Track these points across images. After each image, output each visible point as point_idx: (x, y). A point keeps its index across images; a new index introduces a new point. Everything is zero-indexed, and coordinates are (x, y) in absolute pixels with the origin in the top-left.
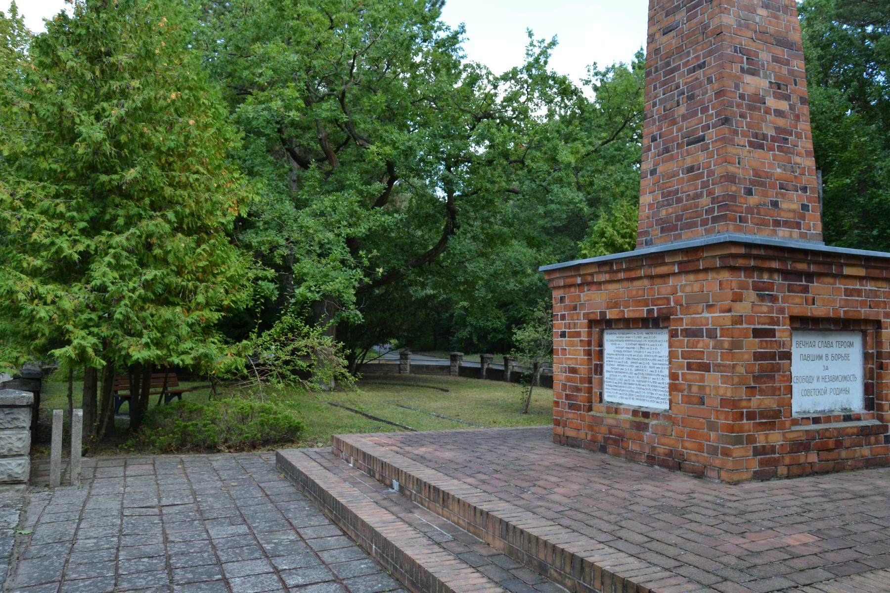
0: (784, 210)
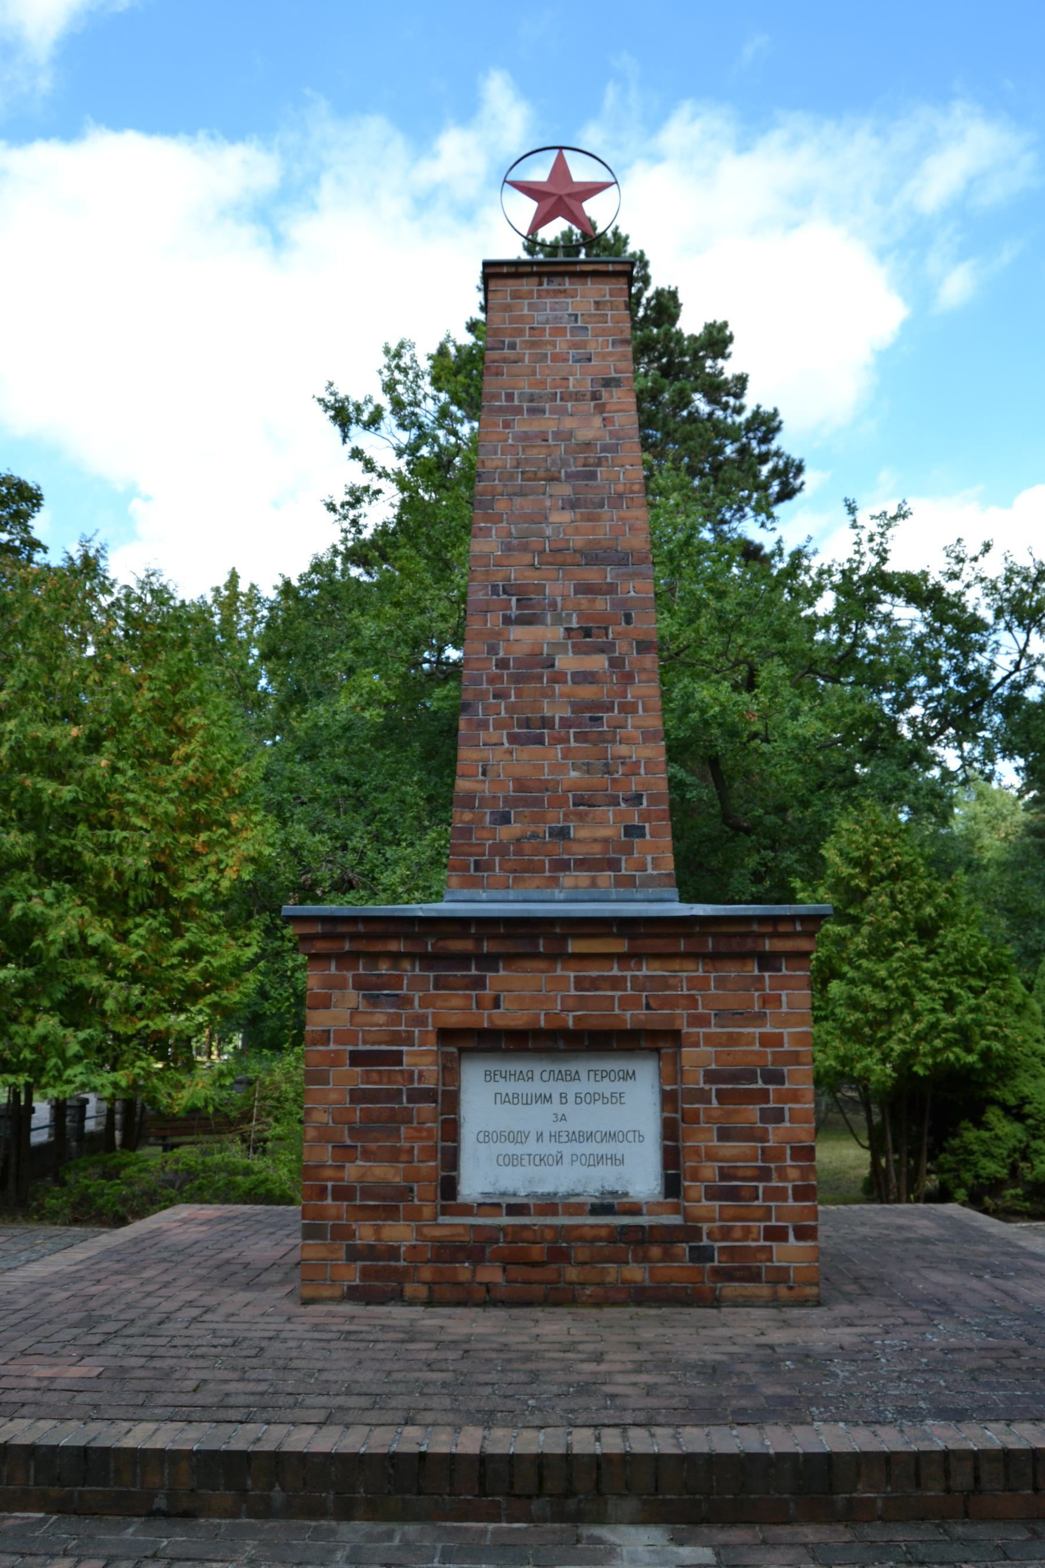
0: (579, 841)
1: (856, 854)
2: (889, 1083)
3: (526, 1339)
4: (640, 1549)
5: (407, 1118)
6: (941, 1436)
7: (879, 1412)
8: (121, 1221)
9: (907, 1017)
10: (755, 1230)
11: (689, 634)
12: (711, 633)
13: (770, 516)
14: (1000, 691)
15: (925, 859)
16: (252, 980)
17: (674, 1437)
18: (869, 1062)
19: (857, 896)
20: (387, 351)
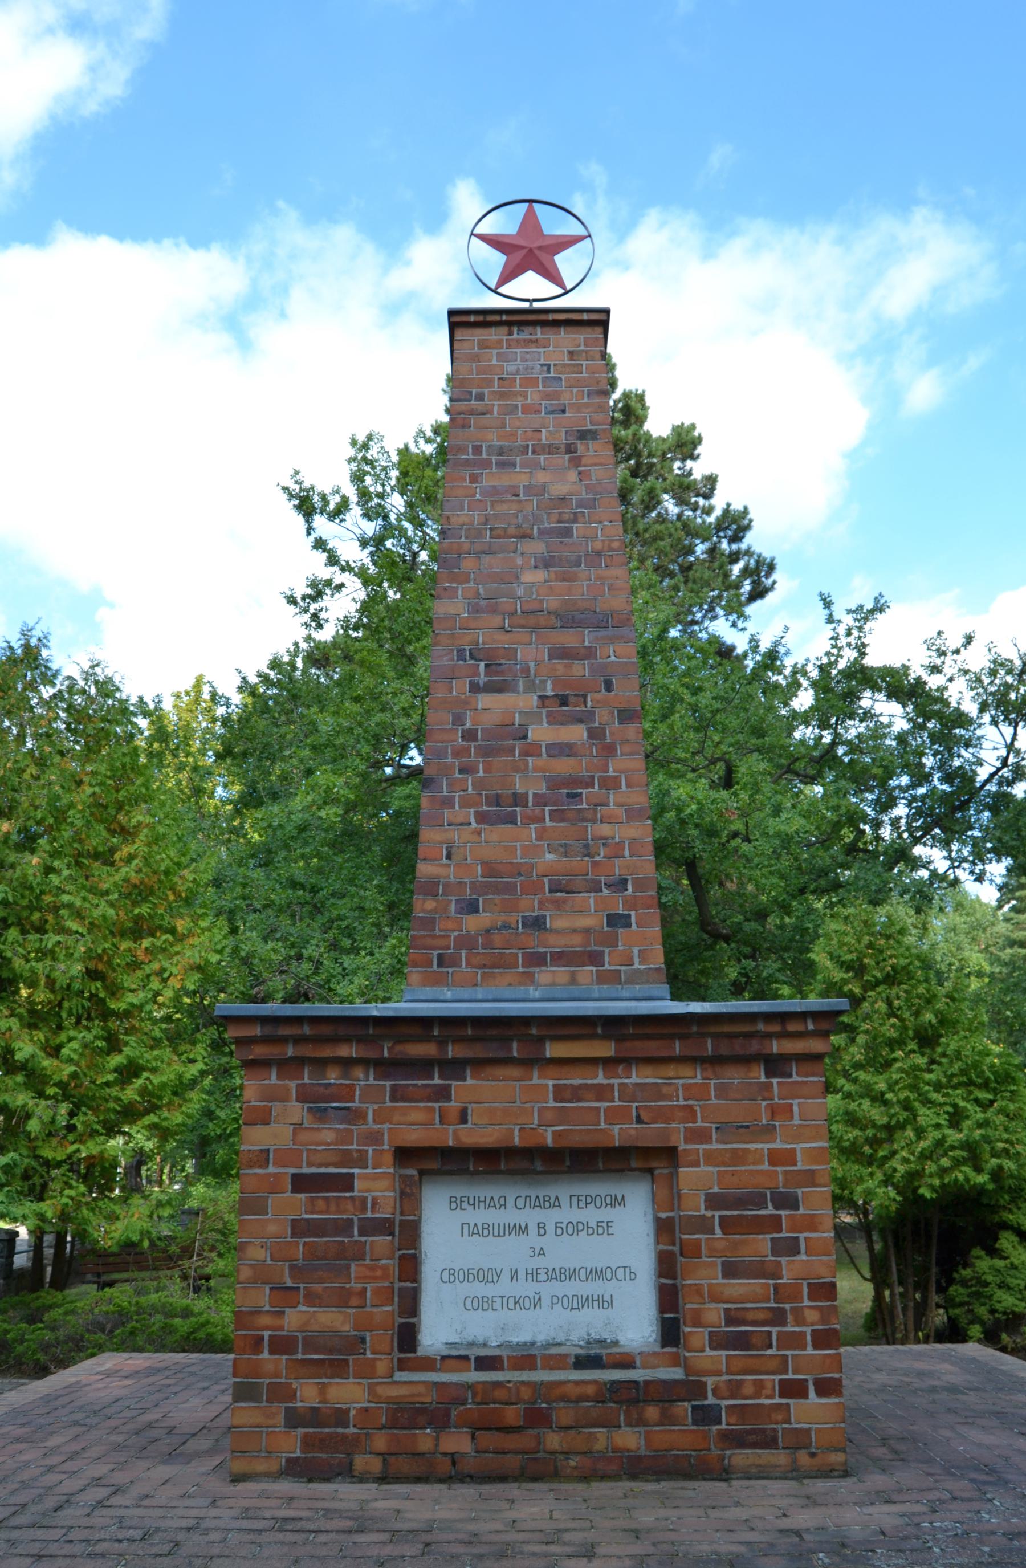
2: (893, 1207)
3: (499, 1526)
8: (42, 1371)
9: (909, 1133)
10: (769, 1385)
13: (741, 615)
14: (987, 787)
16: (196, 1100)
18: (870, 1184)
20: (354, 443)
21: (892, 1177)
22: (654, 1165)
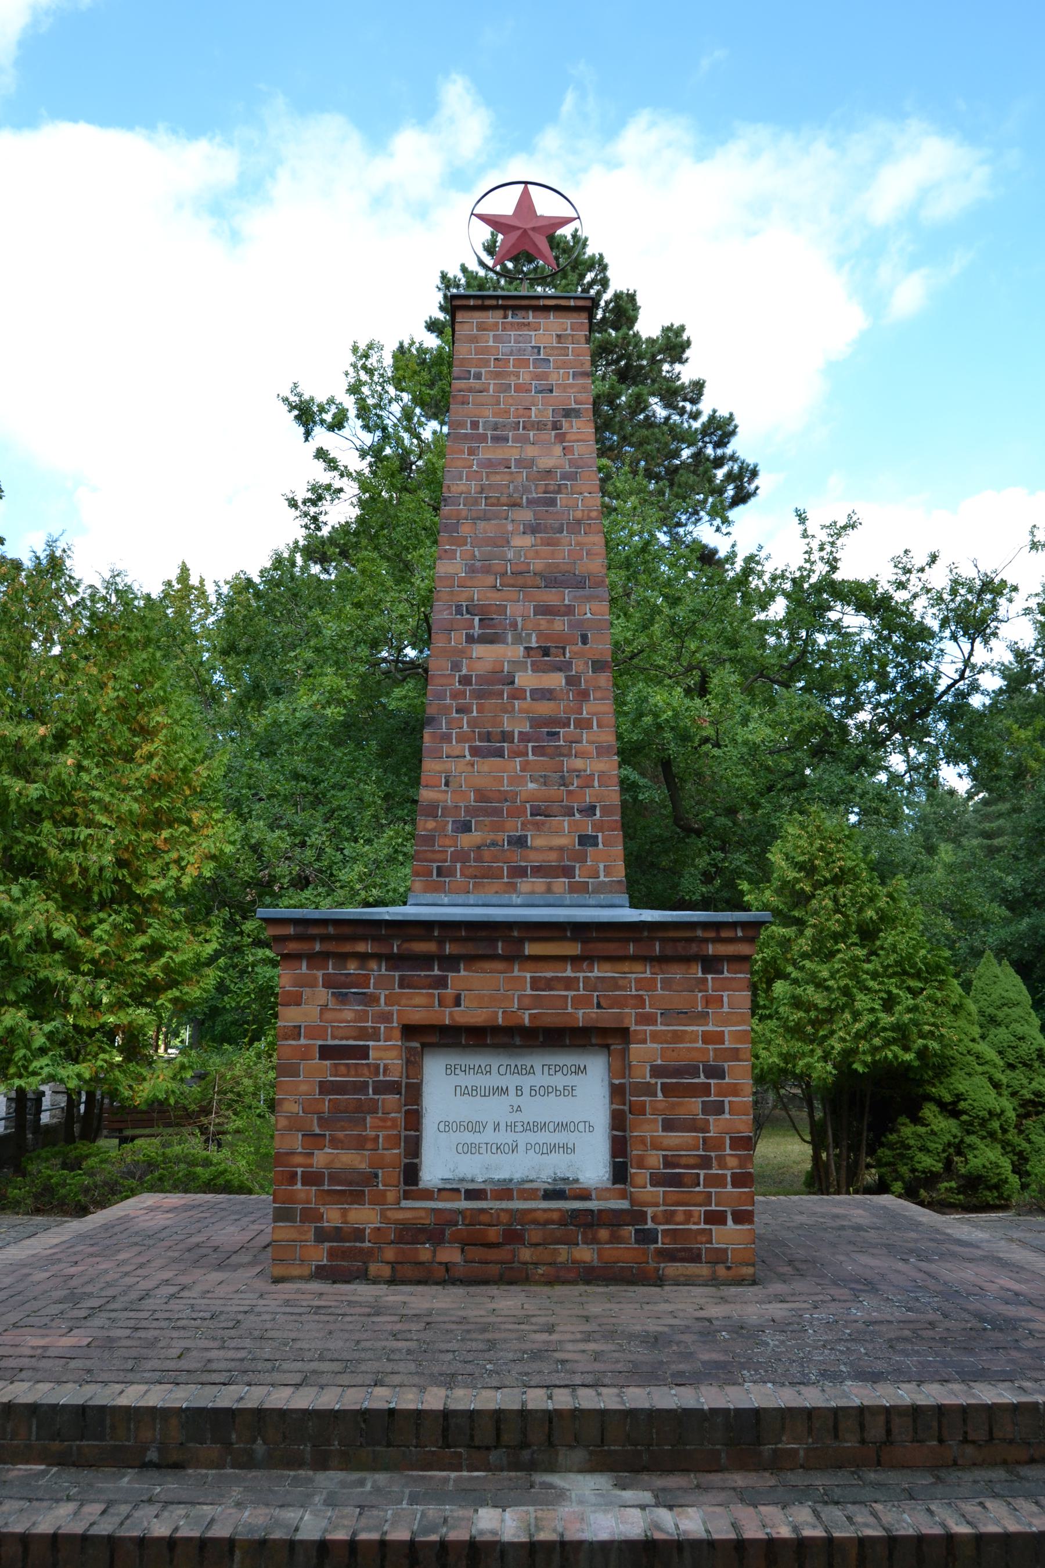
1: (801, 858)
3: (482, 1313)
4: (587, 1493)
5: (373, 1108)
6: (857, 1394)
7: (804, 1375)
8: (82, 1211)
9: (847, 1016)
11: (643, 639)
12: (664, 637)
13: (726, 521)
14: (944, 698)
15: (867, 864)
16: (211, 976)
17: (619, 1395)
19: (802, 899)
20: (355, 350)
21: (829, 1053)
22: (610, 1042)
